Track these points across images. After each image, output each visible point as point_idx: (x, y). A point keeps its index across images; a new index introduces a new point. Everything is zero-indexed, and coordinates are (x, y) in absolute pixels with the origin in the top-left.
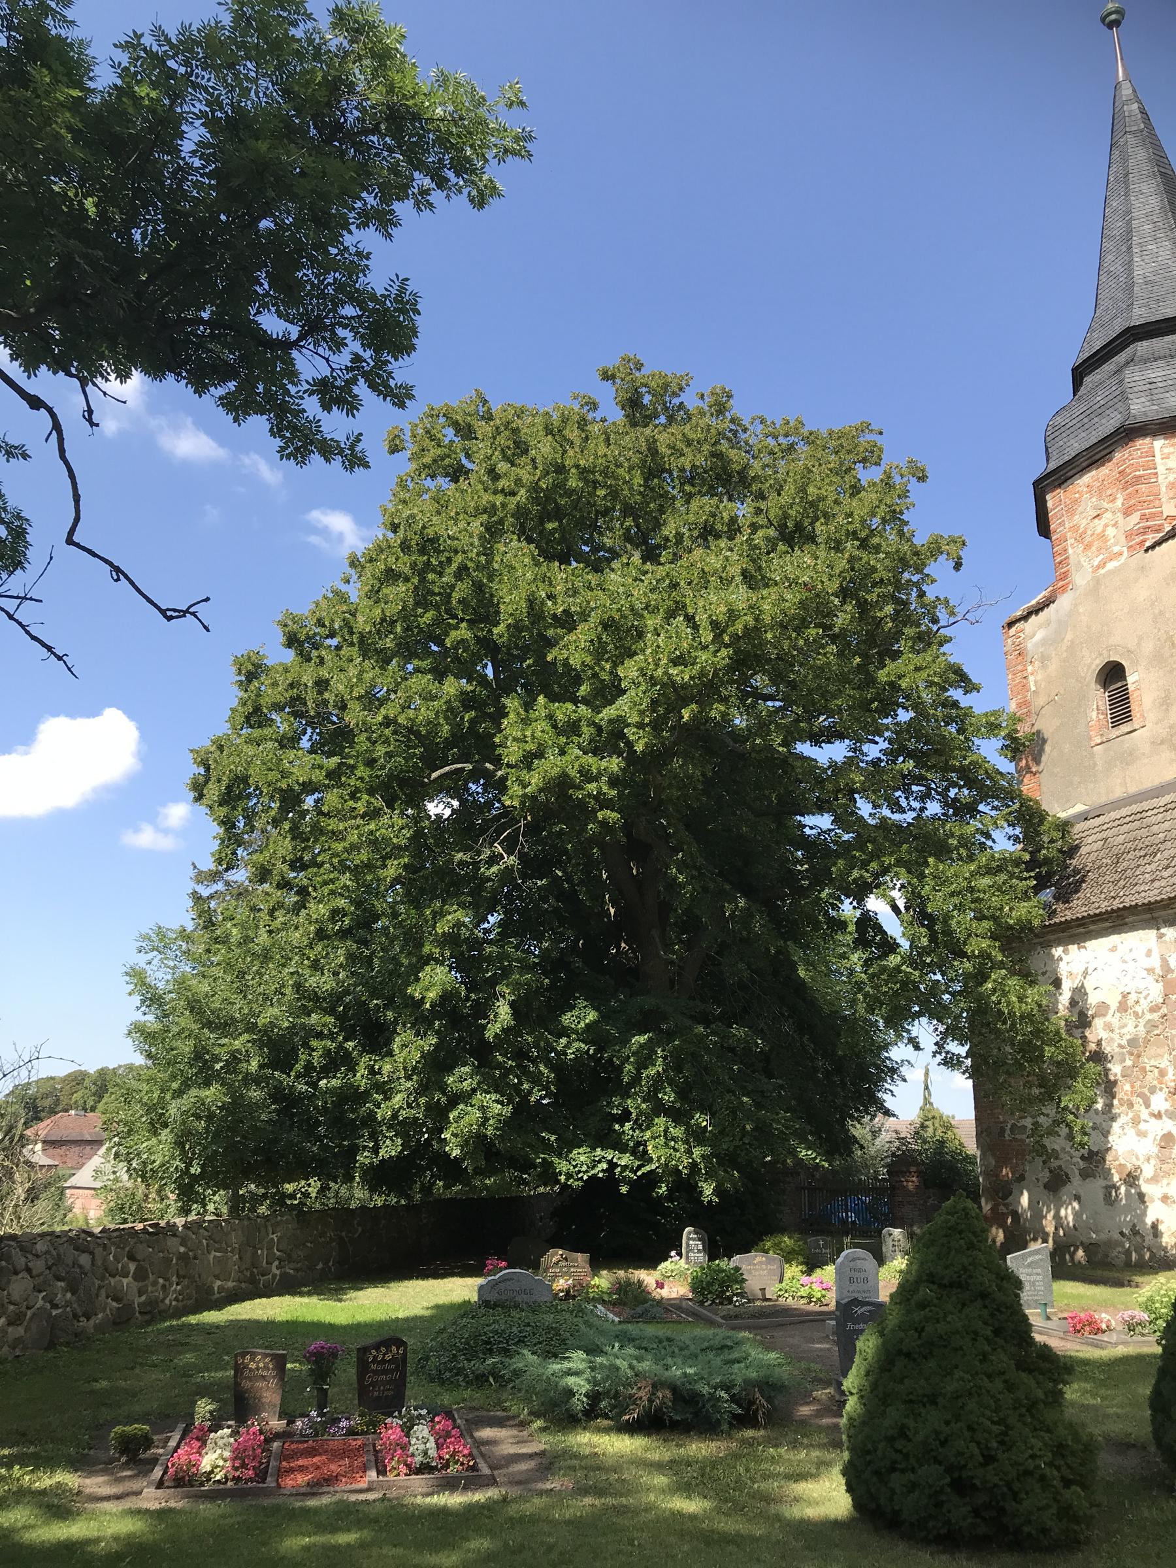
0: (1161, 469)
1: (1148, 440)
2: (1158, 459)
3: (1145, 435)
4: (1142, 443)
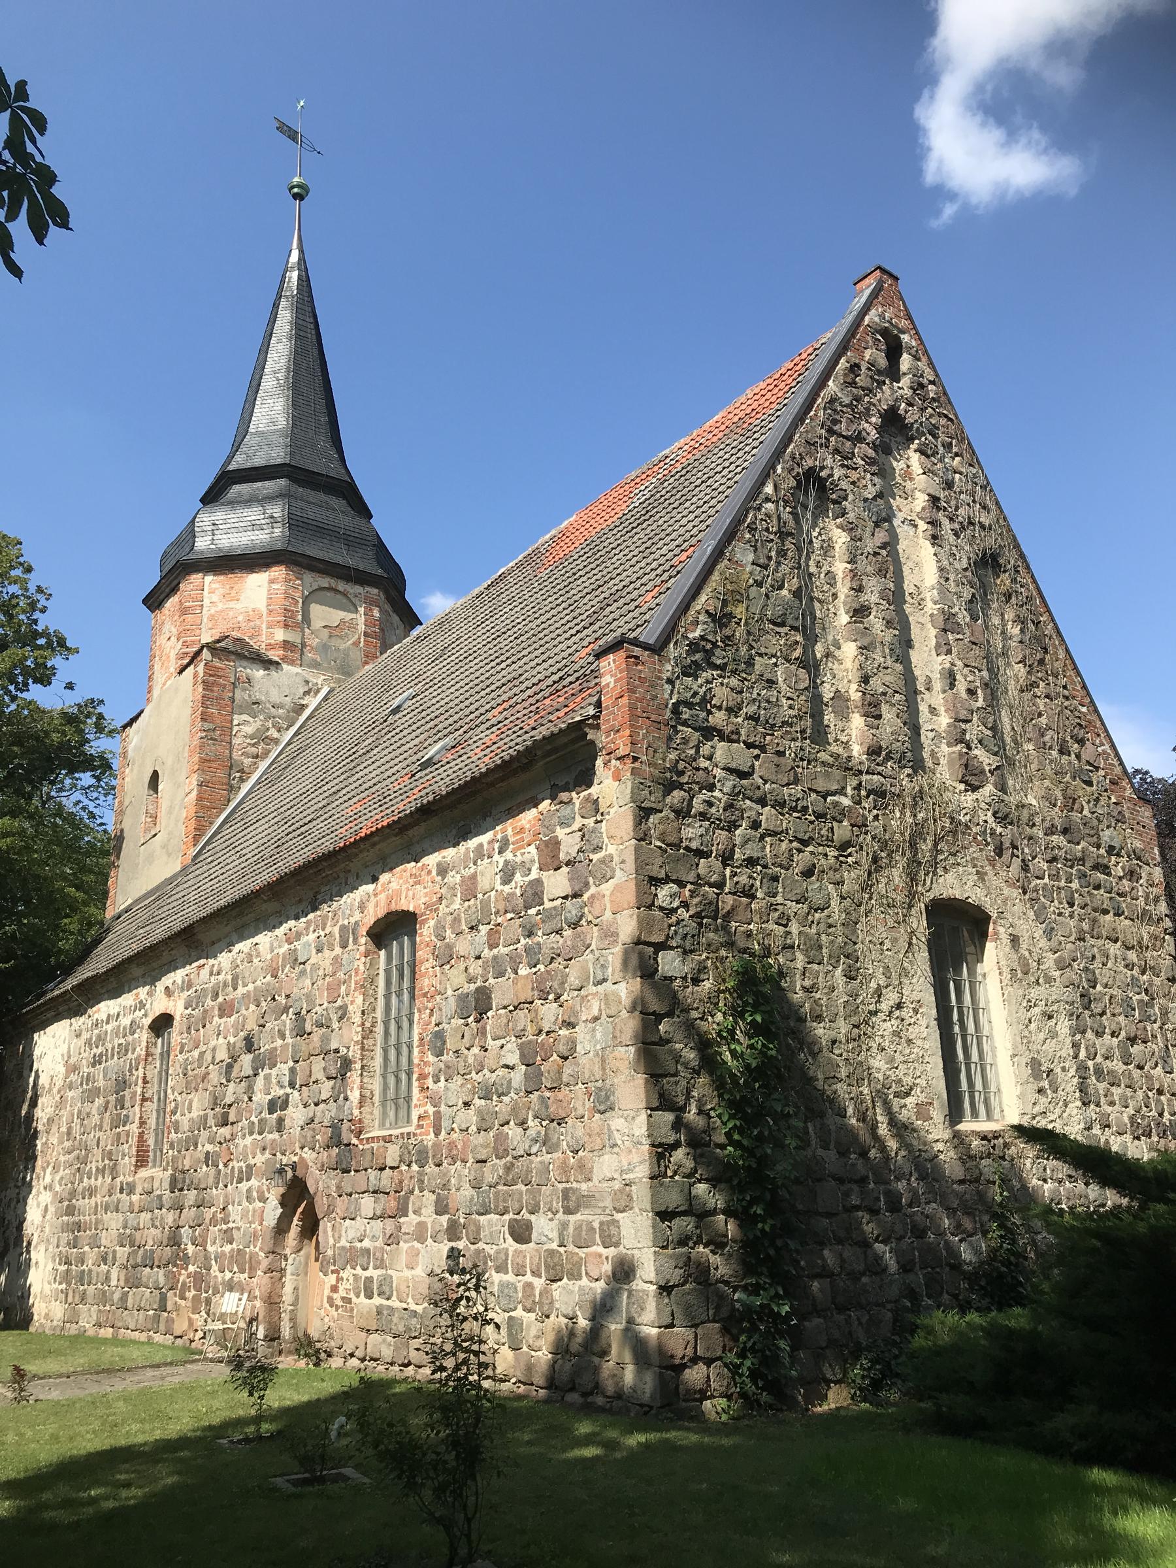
0: (206, 602)
1: (200, 575)
2: (206, 593)
3: (198, 571)
4: (196, 578)
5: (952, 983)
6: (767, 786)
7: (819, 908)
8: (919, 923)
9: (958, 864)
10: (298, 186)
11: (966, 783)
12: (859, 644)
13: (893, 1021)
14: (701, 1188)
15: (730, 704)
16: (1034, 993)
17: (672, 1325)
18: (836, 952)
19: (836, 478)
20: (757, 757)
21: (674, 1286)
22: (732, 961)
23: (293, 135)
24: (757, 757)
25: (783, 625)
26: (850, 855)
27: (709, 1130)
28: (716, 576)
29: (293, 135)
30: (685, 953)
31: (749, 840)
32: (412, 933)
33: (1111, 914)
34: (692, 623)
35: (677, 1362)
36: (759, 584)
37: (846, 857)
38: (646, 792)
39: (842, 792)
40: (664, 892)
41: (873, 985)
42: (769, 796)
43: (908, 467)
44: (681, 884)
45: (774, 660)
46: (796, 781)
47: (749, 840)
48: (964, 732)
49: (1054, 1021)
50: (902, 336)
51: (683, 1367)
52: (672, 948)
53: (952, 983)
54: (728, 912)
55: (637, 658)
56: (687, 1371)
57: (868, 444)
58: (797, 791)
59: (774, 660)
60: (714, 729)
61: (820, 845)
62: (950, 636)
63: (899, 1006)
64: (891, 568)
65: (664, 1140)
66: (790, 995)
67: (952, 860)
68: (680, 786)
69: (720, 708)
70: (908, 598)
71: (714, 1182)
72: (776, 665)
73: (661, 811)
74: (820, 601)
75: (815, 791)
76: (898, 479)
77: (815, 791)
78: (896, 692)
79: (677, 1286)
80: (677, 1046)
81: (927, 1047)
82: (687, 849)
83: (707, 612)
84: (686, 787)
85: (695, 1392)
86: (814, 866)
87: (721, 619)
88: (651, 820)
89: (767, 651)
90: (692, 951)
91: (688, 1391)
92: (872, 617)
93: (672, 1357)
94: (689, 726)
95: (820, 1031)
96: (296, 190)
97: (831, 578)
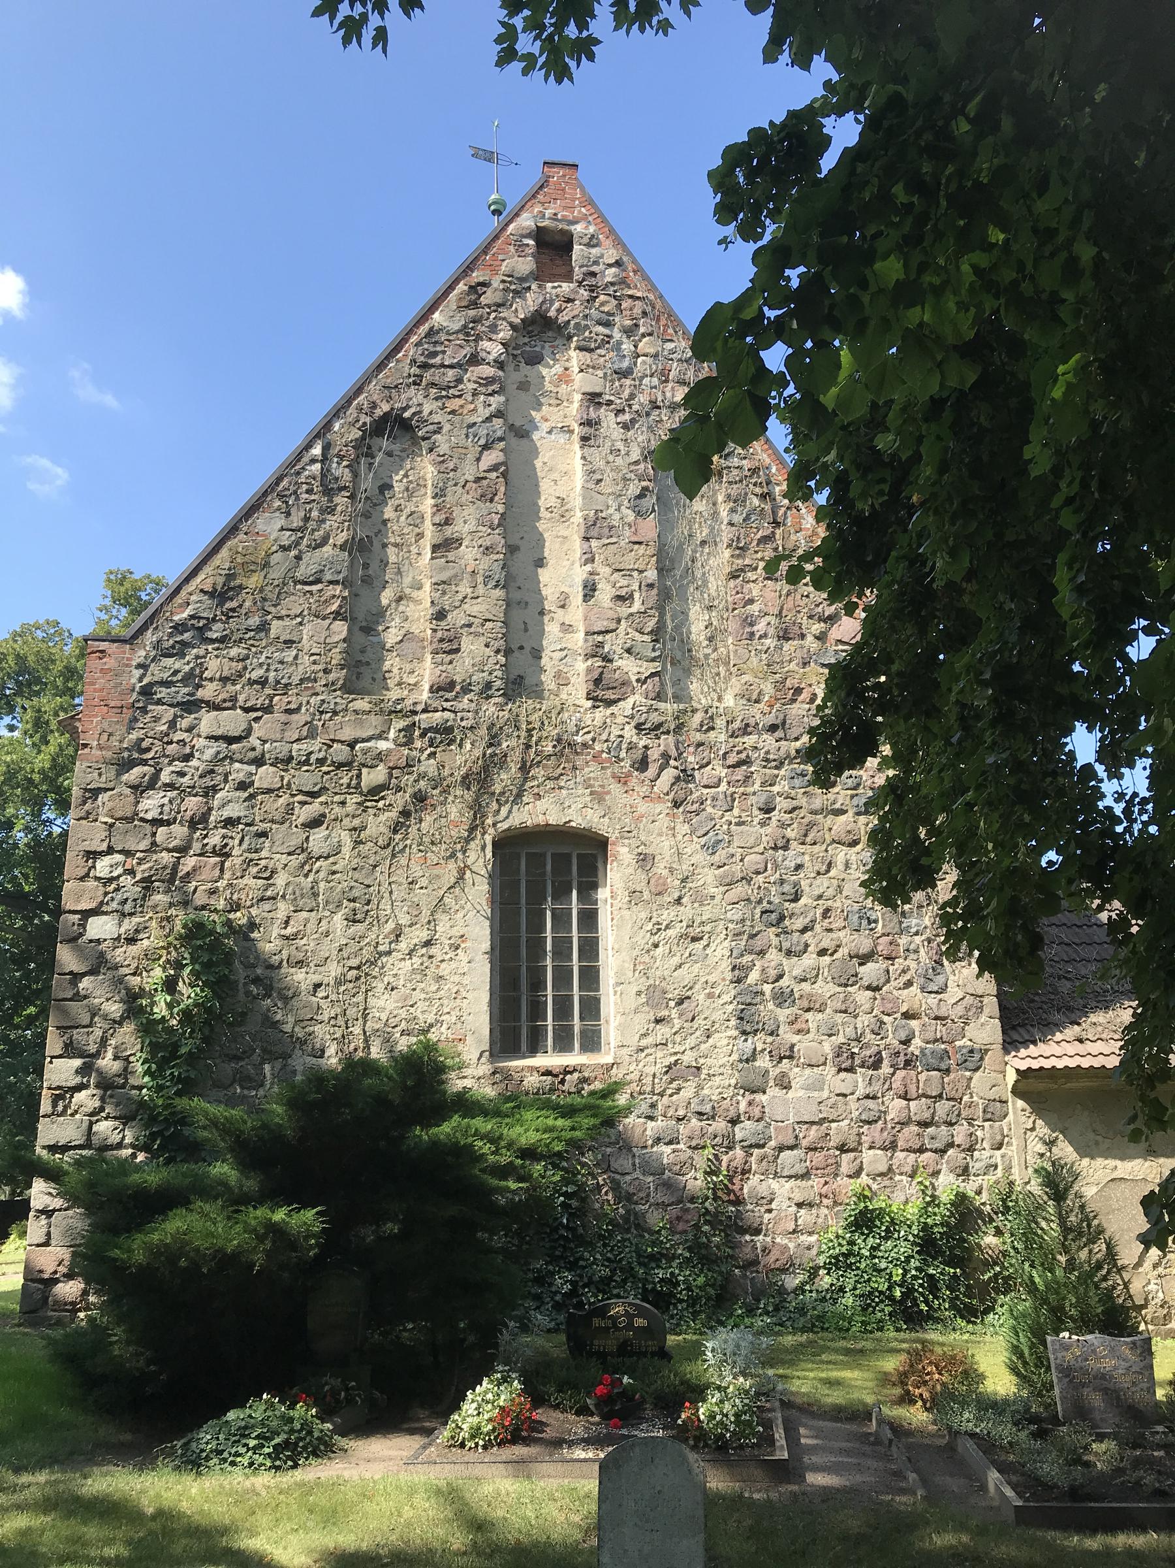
5: (549, 913)
6: (267, 746)
7: (320, 857)
8: (480, 858)
9: (561, 788)
10: (494, 203)
11: (595, 699)
12: (434, 580)
13: (415, 959)
14: (104, 1127)
15: (225, 674)
16: (666, 916)
17: (46, 1244)
18: (336, 895)
19: (425, 413)
20: (257, 719)
21: (54, 1210)
22: (180, 918)
23: (489, 156)
24: (257, 719)
25: (318, 581)
26: (383, 798)
27: (126, 1072)
28: (224, 553)
29: (489, 156)
30: (124, 915)
31: (229, 801)
32: (590, 883)
33: (850, 813)
34: (180, 606)
35: (46, 1276)
36: (284, 548)
37: (377, 801)
38: (96, 774)
39: (381, 736)
40: (103, 863)
41: (391, 925)
42: (267, 756)
43: (566, 369)
44: (128, 853)
45: (299, 620)
46: (312, 735)
47: (229, 801)
48: (600, 645)
49: (704, 942)
50: (572, 228)
51: (53, 1281)
52: (106, 913)
53: (549, 913)
54: (188, 873)
55: (102, 652)
56: (60, 1285)
57: (488, 364)
58: (315, 745)
59: (299, 620)
60: (202, 701)
61: (336, 794)
62: (594, 543)
63: (428, 943)
64: (503, 489)
65: (64, 1084)
66: (260, 945)
67: (550, 784)
68: (144, 762)
69: (211, 680)
70: (543, 513)
71: (125, 1119)
72: (301, 624)
73: (113, 789)
74: (396, 545)
75: (339, 741)
76: (548, 386)
77: (339, 741)
78: (486, 620)
79: (59, 1210)
80: (96, 1001)
81: (465, 982)
82: (143, 820)
83: (202, 591)
84: (151, 762)
85: (66, 1304)
86: (324, 815)
87: (220, 595)
88: (100, 799)
89: (289, 612)
90: (131, 914)
91: (56, 1302)
92: (463, 547)
93: (41, 1271)
94: (164, 704)
95: (301, 978)
96: (492, 208)
97: (416, 519)
